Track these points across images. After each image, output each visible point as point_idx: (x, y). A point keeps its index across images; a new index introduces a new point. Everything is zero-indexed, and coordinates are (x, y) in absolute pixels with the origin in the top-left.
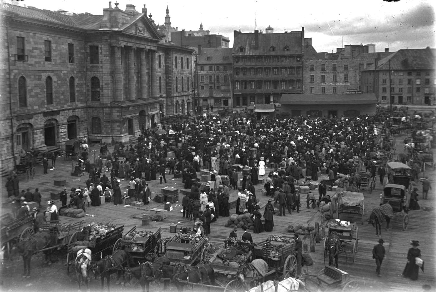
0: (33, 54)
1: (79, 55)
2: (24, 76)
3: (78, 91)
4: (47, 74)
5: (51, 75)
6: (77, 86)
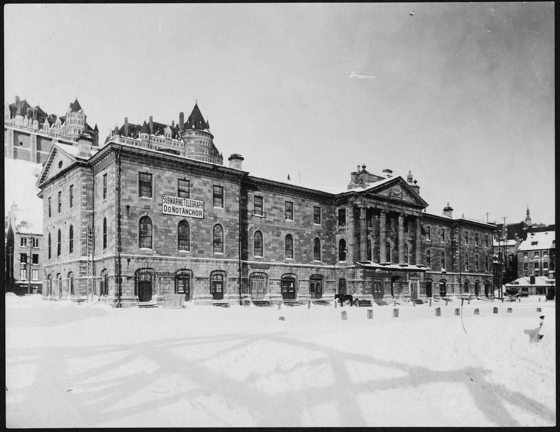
0: (272, 212)
1: (327, 219)
2: (260, 230)
3: (323, 252)
4: (288, 232)
5: (292, 233)
6: (323, 248)
